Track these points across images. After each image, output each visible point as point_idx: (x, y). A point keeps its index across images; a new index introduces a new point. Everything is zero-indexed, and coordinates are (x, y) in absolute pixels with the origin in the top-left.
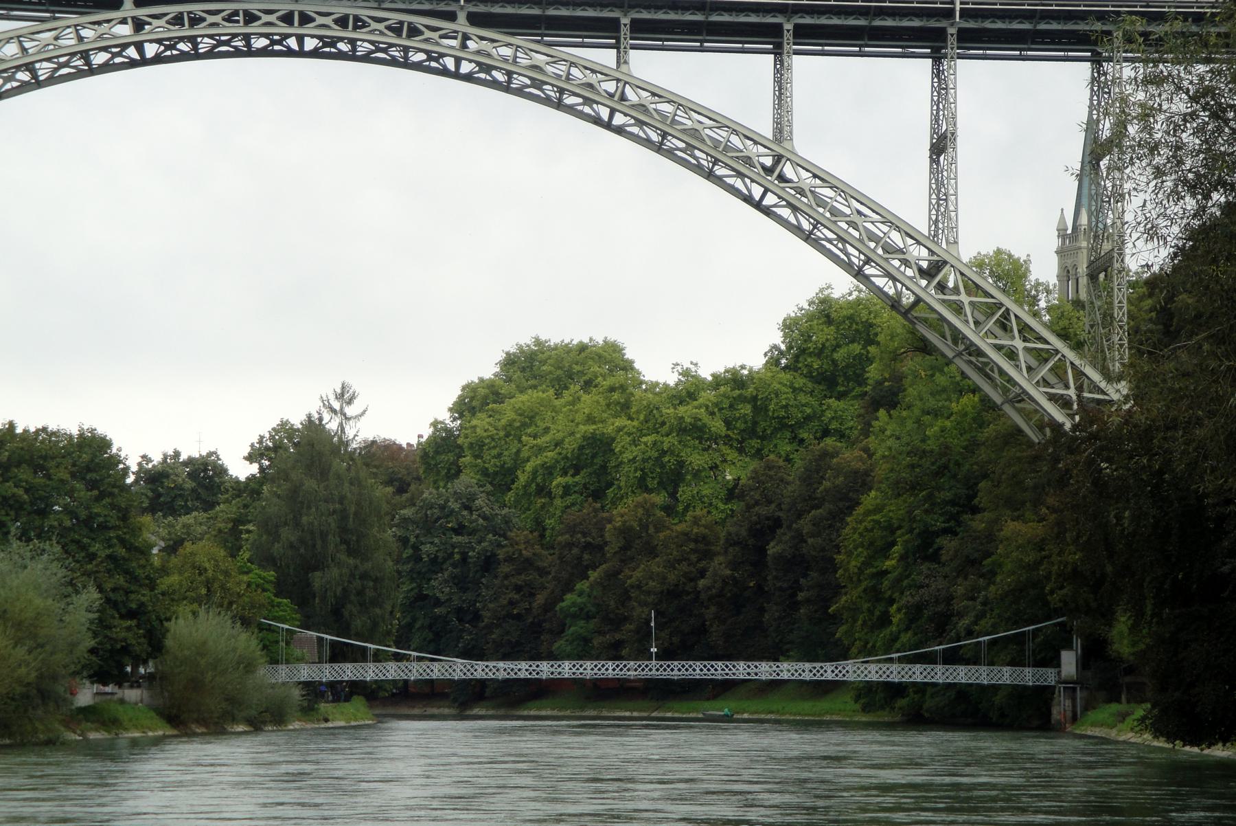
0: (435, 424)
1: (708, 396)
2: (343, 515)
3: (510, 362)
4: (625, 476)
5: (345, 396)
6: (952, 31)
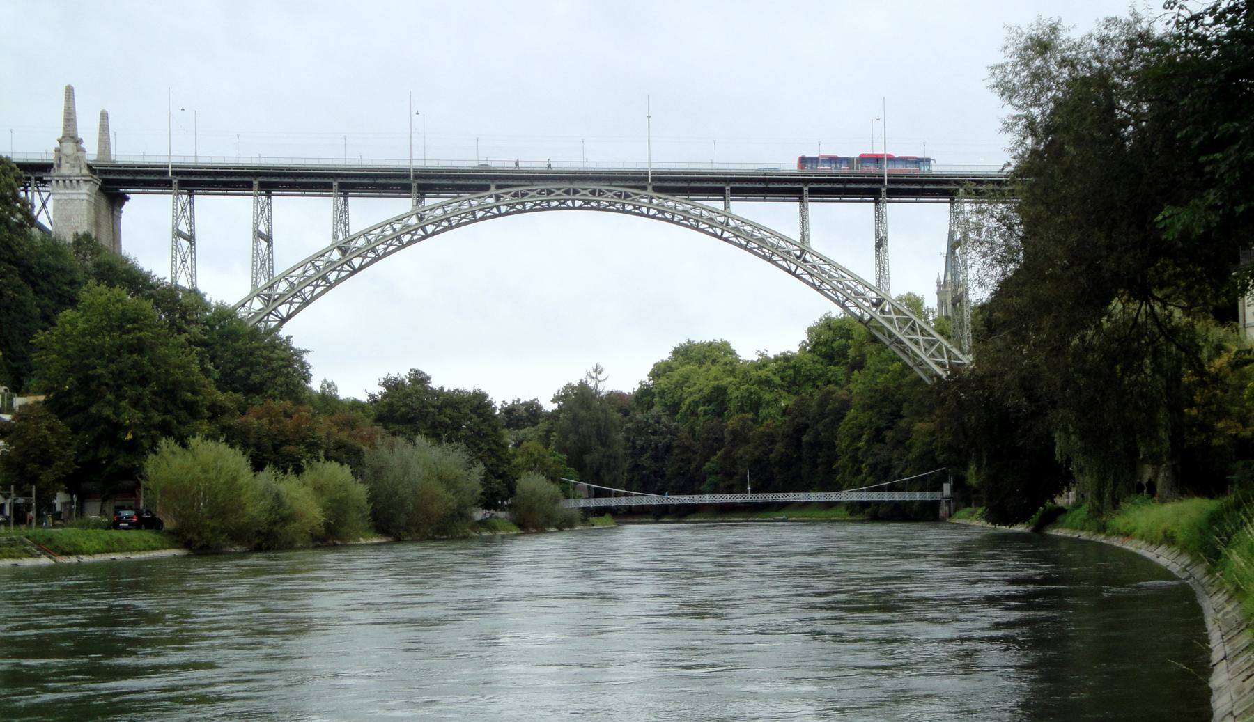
0: (641, 383)
2: (599, 427)
3: (676, 352)
4: (733, 405)
5: (598, 370)
6: (884, 189)
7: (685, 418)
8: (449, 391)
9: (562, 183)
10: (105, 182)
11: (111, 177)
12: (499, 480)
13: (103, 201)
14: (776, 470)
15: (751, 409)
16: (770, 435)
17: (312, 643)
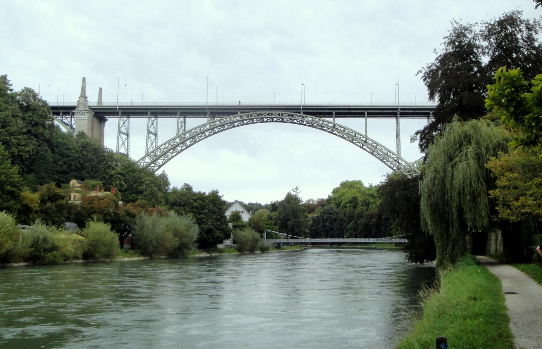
0: (329, 195)
1: (374, 189)
2: (293, 211)
3: (341, 184)
4: (360, 203)
5: (297, 189)
6: (398, 113)
7: (342, 209)
9: (267, 111)
10: (96, 113)
11: (98, 111)
12: (220, 232)
13: (96, 121)
14: (373, 228)
15: (366, 205)
16: (372, 215)
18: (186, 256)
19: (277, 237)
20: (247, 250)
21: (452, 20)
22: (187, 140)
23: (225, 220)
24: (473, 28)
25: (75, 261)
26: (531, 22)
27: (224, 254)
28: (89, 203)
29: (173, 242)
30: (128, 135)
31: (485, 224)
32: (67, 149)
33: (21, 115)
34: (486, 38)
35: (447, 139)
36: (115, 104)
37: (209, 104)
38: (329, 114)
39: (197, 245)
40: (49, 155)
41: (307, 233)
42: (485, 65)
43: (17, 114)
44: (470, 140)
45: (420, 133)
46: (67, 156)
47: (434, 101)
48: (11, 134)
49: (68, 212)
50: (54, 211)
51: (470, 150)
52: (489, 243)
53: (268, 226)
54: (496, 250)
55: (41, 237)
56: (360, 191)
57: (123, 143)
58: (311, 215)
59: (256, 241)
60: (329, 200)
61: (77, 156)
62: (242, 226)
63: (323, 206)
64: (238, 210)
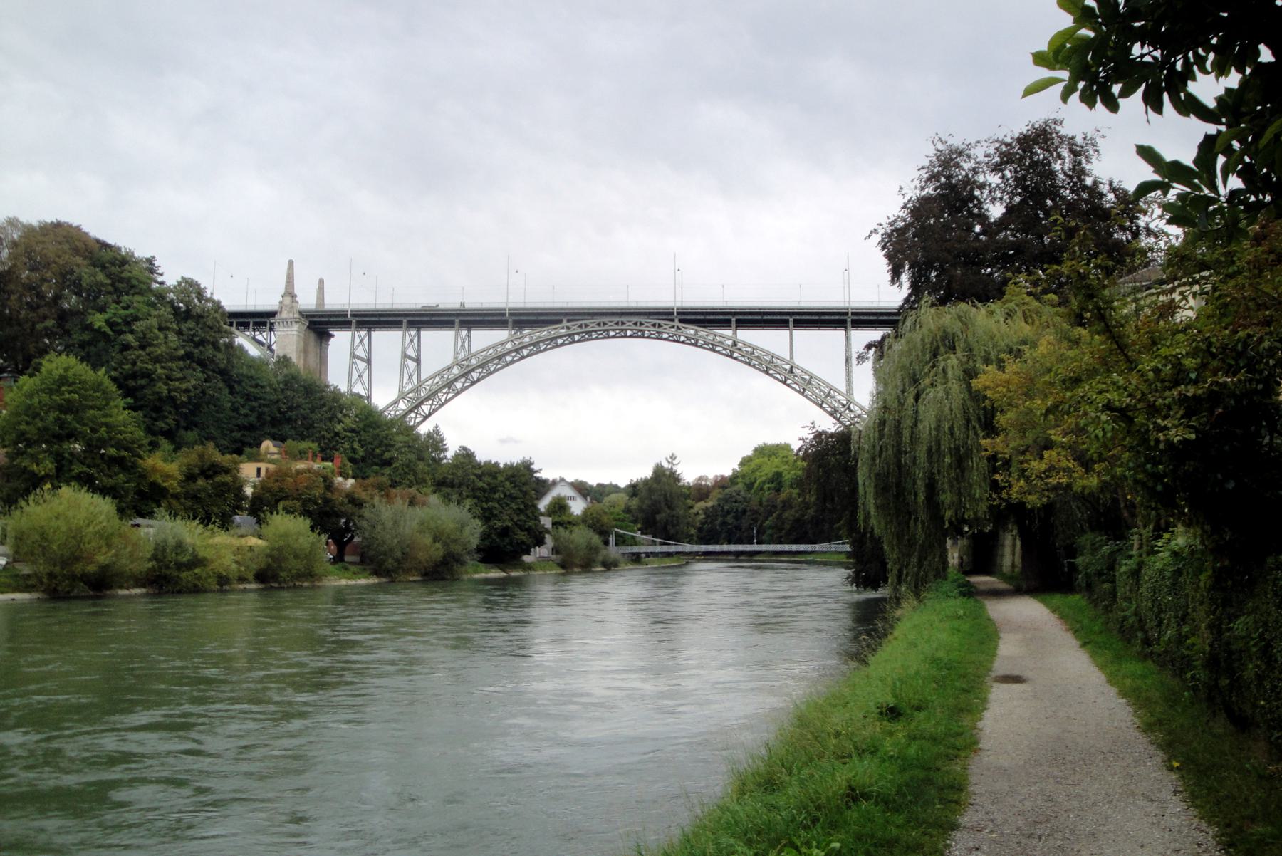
2: (665, 495)
3: (756, 450)
5: (673, 457)
6: (849, 320)
7: (756, 493)
8: (506, 465)
10: (310, 322)
13: (312, 337)
17: (529, 630)
18: (456, 577)
19: (634, 542)
20: (577, 566)
21: (934, 135)
22: (473, 370)
23: (533, 513)
24: (972, 152)
25: (241, 586)
26: (1079, 140)
27: (533, 573)
28: (277, 481)
29: (431, 551)
30: (368, 362)
31: (980, 514)
32: (257, 386)
33: (175, 326)
34: (997, 168)
35: (908, 342)
36: (346, 307)
37: (512, 305)
38: (725, 323)
39: (476, 556)
40: (225, 399)
41: (692, 535)
42: (995, 222)
43: (168, 324)
44: (953, 343)
45: (876, 346)
46: (256, 399)
47: (900, 285)
48: (156, 360)
49: (236, 495)
50: (210, 496)
51: (952, 362)
52: (1000, 553)
53: (619, 523)
54: (1013, 566)
55: (171, 541)
56: (787, 462)
57: (360, 376)
58: (701, 505)
59: (596, 550)
60: (734, 479)
61: (274, 397)
62: (569, 523)
63: (724, 487)
64: (562, 494)
